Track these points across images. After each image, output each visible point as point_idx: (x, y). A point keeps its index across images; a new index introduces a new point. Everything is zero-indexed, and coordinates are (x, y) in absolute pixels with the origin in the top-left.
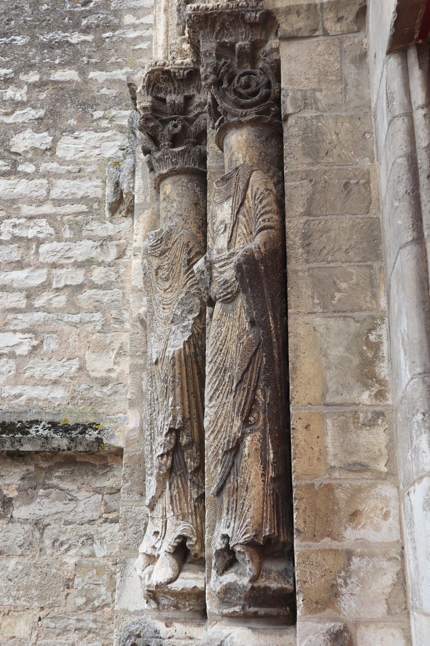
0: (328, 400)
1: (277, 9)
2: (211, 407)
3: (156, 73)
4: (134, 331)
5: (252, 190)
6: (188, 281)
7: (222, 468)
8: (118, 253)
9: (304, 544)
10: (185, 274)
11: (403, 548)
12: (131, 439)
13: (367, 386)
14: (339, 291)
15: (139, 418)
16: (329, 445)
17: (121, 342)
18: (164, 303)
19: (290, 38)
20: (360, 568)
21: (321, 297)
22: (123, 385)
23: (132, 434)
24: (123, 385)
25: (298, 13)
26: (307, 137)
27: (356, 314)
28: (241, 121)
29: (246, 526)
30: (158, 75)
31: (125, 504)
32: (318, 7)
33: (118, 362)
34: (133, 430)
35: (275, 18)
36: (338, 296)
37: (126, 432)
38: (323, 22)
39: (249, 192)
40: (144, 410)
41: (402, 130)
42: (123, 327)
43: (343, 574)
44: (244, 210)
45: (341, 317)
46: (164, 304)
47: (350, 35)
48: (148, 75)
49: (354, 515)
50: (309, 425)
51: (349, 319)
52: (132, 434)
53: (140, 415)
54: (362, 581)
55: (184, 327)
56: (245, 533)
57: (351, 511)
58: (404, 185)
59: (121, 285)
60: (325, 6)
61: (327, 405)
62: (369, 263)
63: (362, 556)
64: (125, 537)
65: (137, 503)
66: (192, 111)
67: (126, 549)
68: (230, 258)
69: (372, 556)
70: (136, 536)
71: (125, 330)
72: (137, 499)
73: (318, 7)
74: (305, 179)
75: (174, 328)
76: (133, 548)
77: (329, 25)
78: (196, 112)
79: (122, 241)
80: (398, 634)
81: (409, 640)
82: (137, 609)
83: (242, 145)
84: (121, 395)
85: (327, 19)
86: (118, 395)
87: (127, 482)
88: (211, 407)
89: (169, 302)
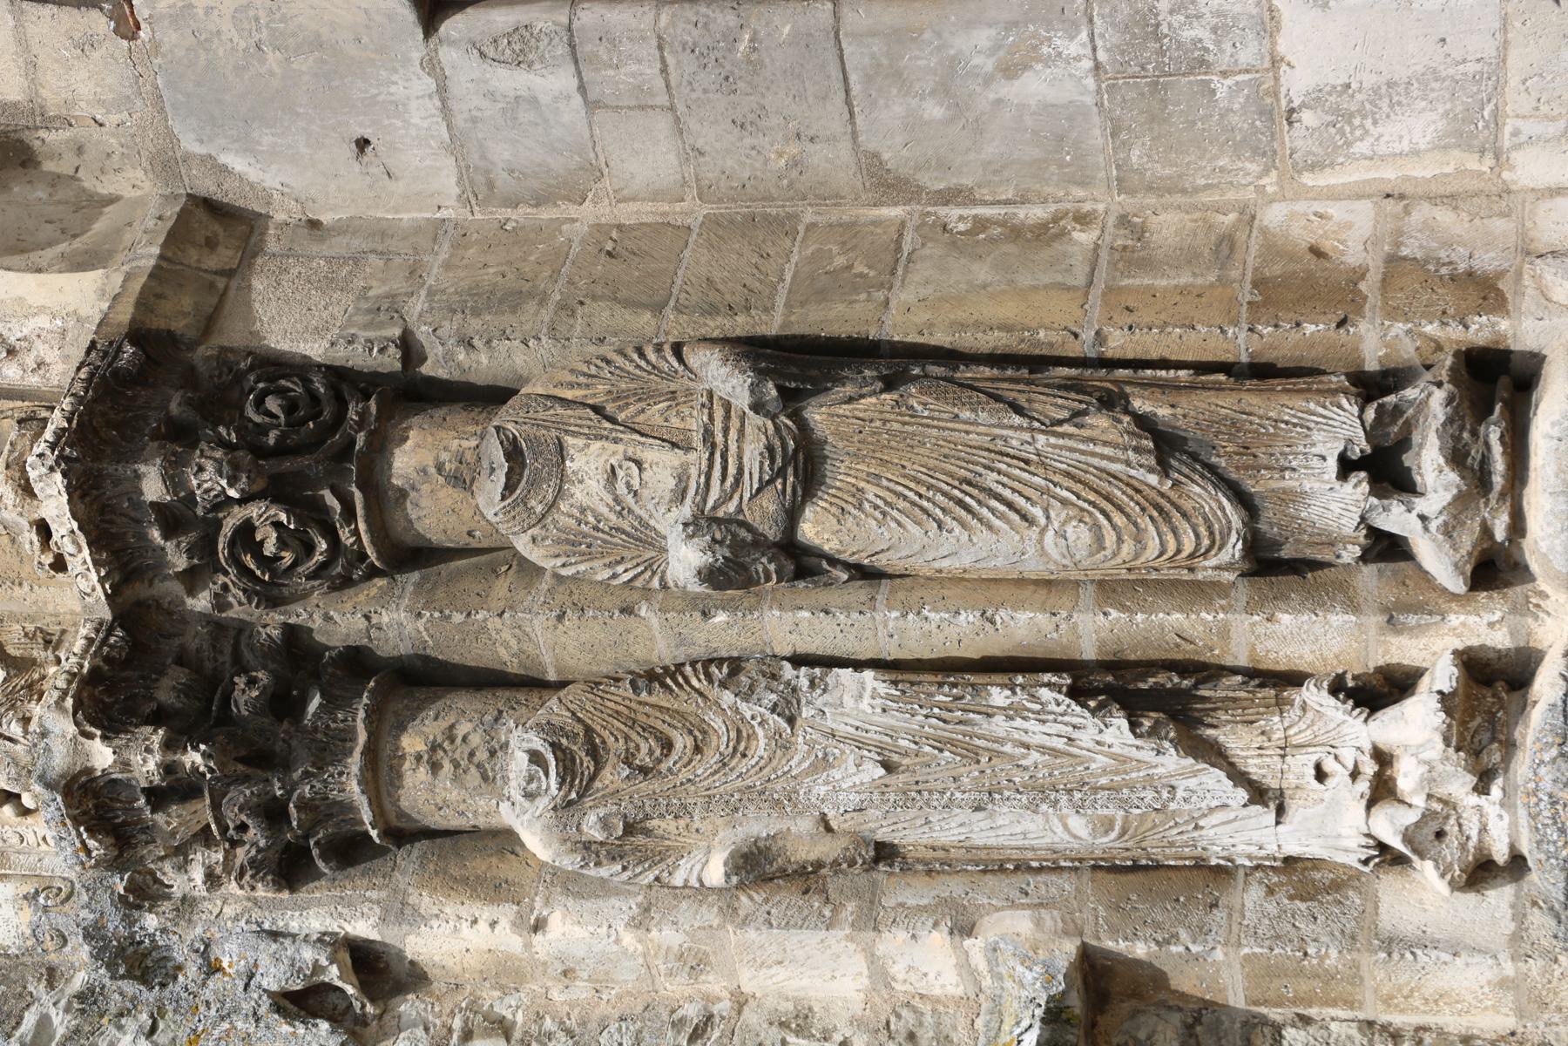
0: (1080, 280)
1: (133, 320)
2: (1048, 518)
3: (85, 694)
4: (761, 920)
5: (571, 386)
6: (692, 687)
7: (1193, 481)
8: (490, 1036)
9: (1368, 314)
10: (671, 691)
11: (1388, 196)
12: (1060, 924)
13: (1063, 234)
14: (850, 267)
15: (1008, 912)
16: (1175, 282)
17: (765, 1026)
18: (731, 749)
19: (209, 323)
20: (1421, 247)
21: (855, 289)
22: (893, 1019)
23: (1049, 923)
24: (893, 1019)
25: (159, 296)
26: (472, 308)
27: (906, 248)
28: (81, 997)
29: (1324, 407)
30: (92, 697)
31: (1233, 940)
32: (165, 265)
33: (825, 1031)
34: (1038, 923)
35: (149, 330)
36: (860, 268)
37: (1039, 936)
38: (199, 269)
39: (569, 394)
40: (986, 901)
41: (603, 11)
42: (723, 1018)
43: (1432, 267)
44: (610, 408)
45: (906, 266)
46: (735, 749)
47: (253, 240)
48: (80, 715)
49: (1317, 252)
50: (1127, 308)
51: (914, 257)
52: (1049, 923)
53: (997, 910)
54: (1447, 244)
55: (812, 685)
56: (1340, 407)
57: (1309, 256)
58: (718, 15)
59: (593, 1026)
60: (170, 254)
61: (1090, 283)
62: (801, 228)
63: (1398, 245)
64: (1323, 939)
65: (1236, 916)
66: (215, 669)
67: (1353, 938)
68: (714, 445)
69: (1399, 233)
70: (1321, 918)
71: (734, 1014)
72: (1224, 915)
73: (165, 265)
74: (573, 311)
75: (806, 712)
76: (1353, 923)
77: (212, 262)
78: (228, 650)
79: (457, 1024)
80: (1544, 206)
81: (1556, 191)
82: (1509, 916)
83: (430, 439)
84: (921, 1024)
85: (199, 261)
86: (919, 1033)
87: (1176, 936)
88: (1048, 518)
89: (733, 735)
